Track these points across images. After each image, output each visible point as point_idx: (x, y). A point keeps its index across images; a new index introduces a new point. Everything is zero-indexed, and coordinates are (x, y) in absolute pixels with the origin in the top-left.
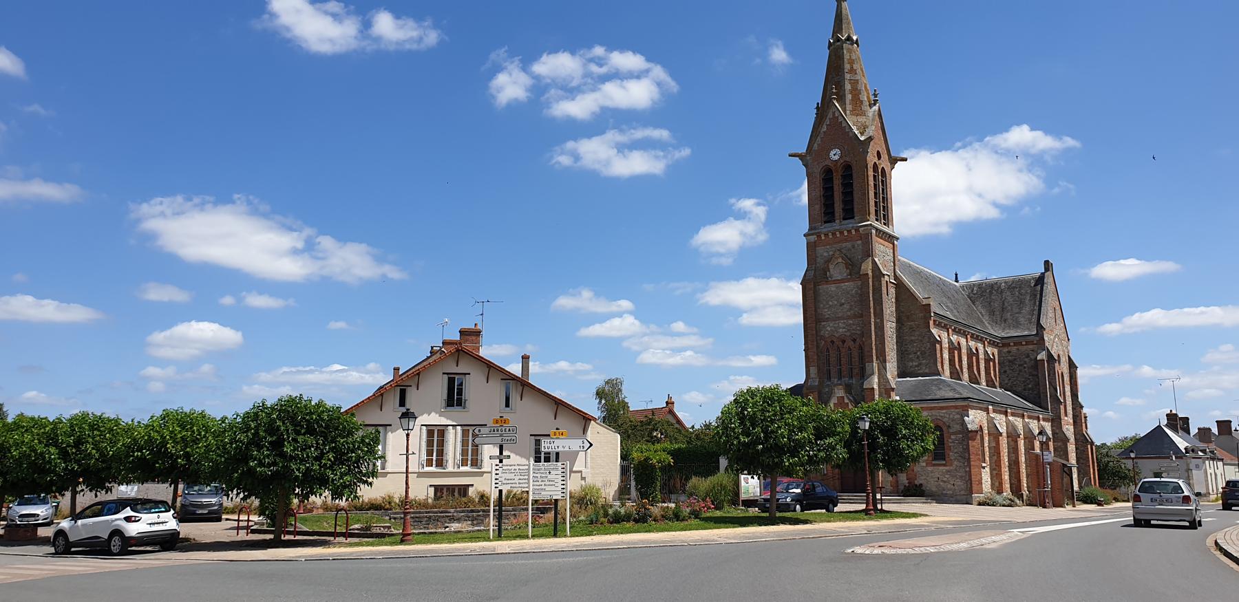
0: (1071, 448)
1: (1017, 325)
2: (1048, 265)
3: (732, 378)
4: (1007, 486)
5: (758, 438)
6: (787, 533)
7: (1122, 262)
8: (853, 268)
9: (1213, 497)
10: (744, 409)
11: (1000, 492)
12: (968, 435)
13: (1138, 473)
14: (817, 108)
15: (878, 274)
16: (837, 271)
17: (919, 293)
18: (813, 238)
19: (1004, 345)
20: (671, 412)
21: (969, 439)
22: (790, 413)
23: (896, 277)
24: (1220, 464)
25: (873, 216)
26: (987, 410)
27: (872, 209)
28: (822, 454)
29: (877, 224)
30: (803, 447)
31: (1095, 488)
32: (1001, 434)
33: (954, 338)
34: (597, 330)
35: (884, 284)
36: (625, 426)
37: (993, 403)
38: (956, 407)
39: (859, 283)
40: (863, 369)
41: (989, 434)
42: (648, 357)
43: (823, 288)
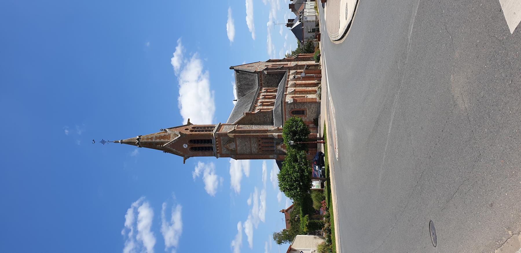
0: (300, 63)
1: (254, 80)
2: (232, 68)
3: (271, 180)
4: (314, 88)
5: (298, 184)
7: (227, 29)
8: (231, 140)
9: (317, 14)
10: (287, 188)
11: (316, 91)
15: (234, 131)
16: (232, 146)
17: (241, 116)
18: (218, 155)
19: (261, 85)
20: (287, 211)
22: (288, 171)
23: (235, 124)
24: (305, 10)
25: (211, 133)
27: (208, 133)
29: (214, 131)
30: (301, 167)
31: (314, 55)
33: (259, 104)
34: (250, 239)
35: (238, 129)
36: (293, 232)
37: (283, 92)
38: (285, 106)
40: (271, 138)
42: (262, 216)
43: (238, 152)
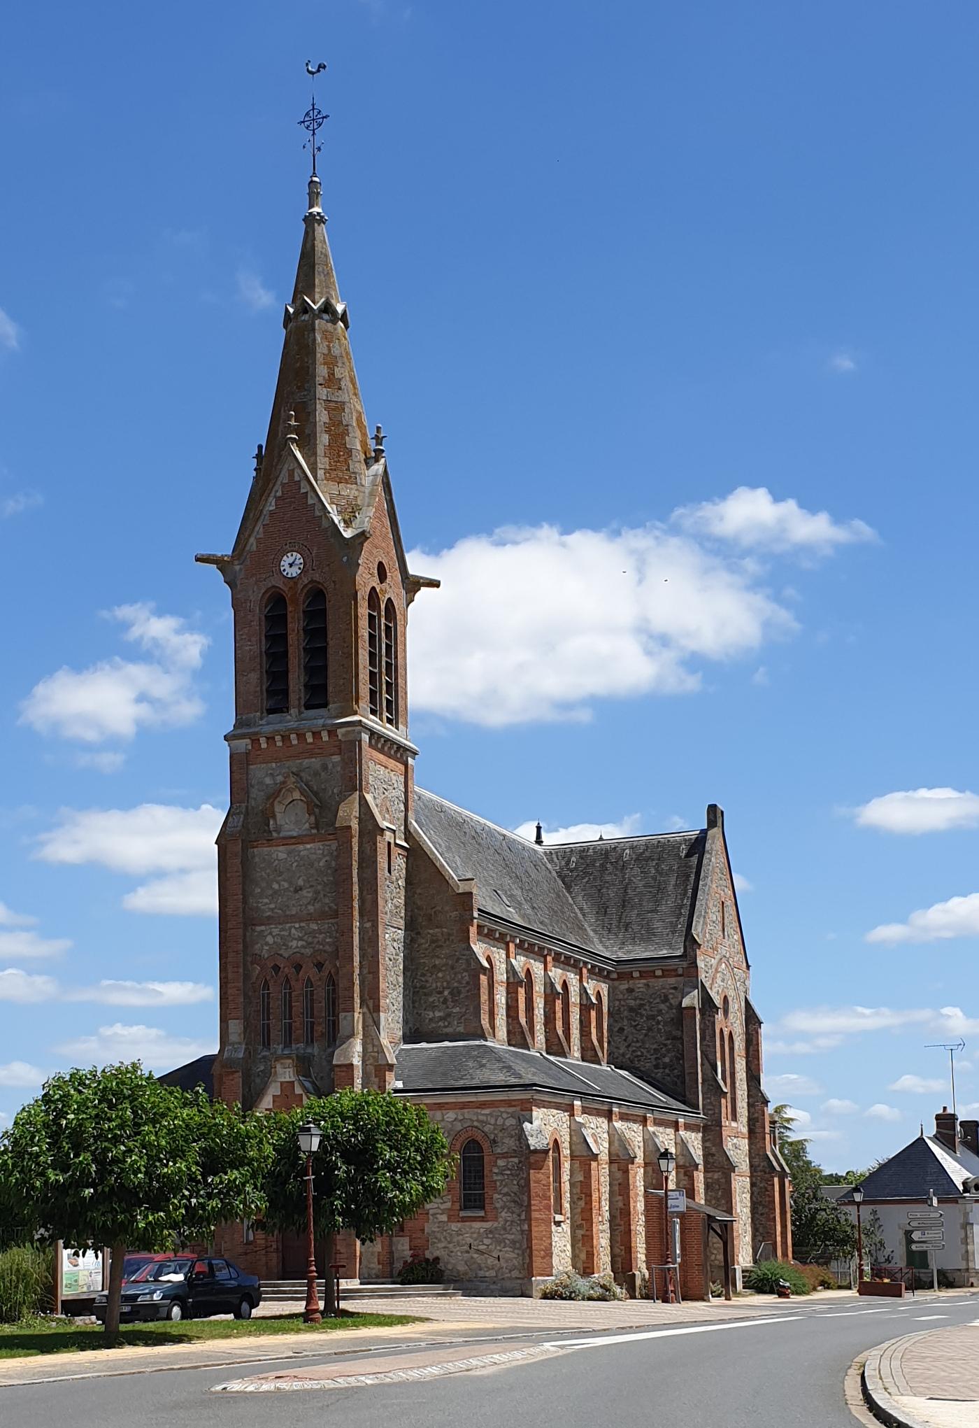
1: (648, 935)
2: (714, 815)
4: (603, 1259)
5: (85, 1173)
6: (144, 1361)
7: (923, 793)
8: (322, 810)
10: (61, 1114)
12: (530, 1159)
13: (859, 1234)
14: (259, 456)
15: (371, 829)
16: (291, 818)
17: (453, 866)
18: (244, 744)
19: (621, 976)
21: (531, 1166)
22: (154, 1122)
23: (408, 835)
25: (365, 704)
26: (570, 1109)
27: (365, 689)
28: (214, 1203)
29: (372, 722)
30: (176, 1189)
31: (784, 1263)
32: (595, 1157)
33: (519, 962)
38: (509, 1103)
39: (334, 845)
41: (573, 1157)
